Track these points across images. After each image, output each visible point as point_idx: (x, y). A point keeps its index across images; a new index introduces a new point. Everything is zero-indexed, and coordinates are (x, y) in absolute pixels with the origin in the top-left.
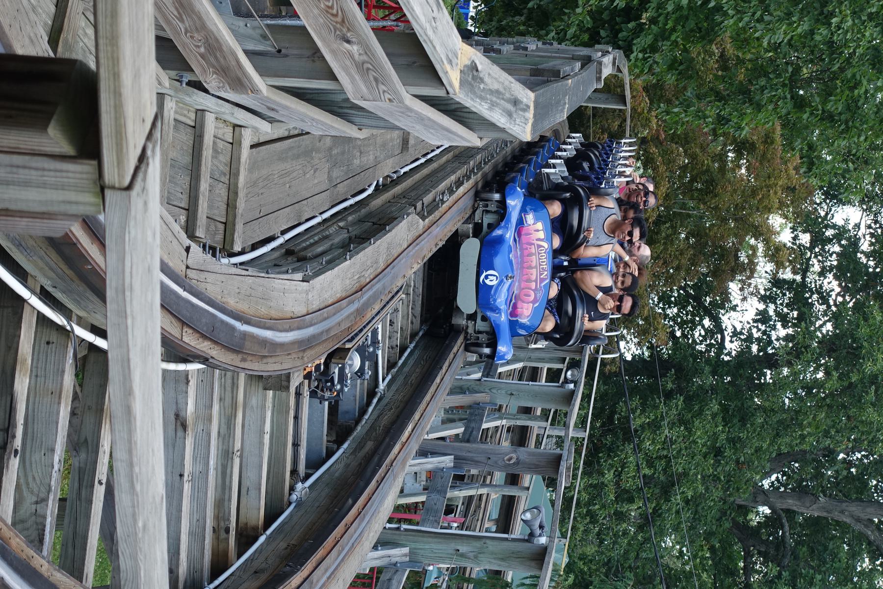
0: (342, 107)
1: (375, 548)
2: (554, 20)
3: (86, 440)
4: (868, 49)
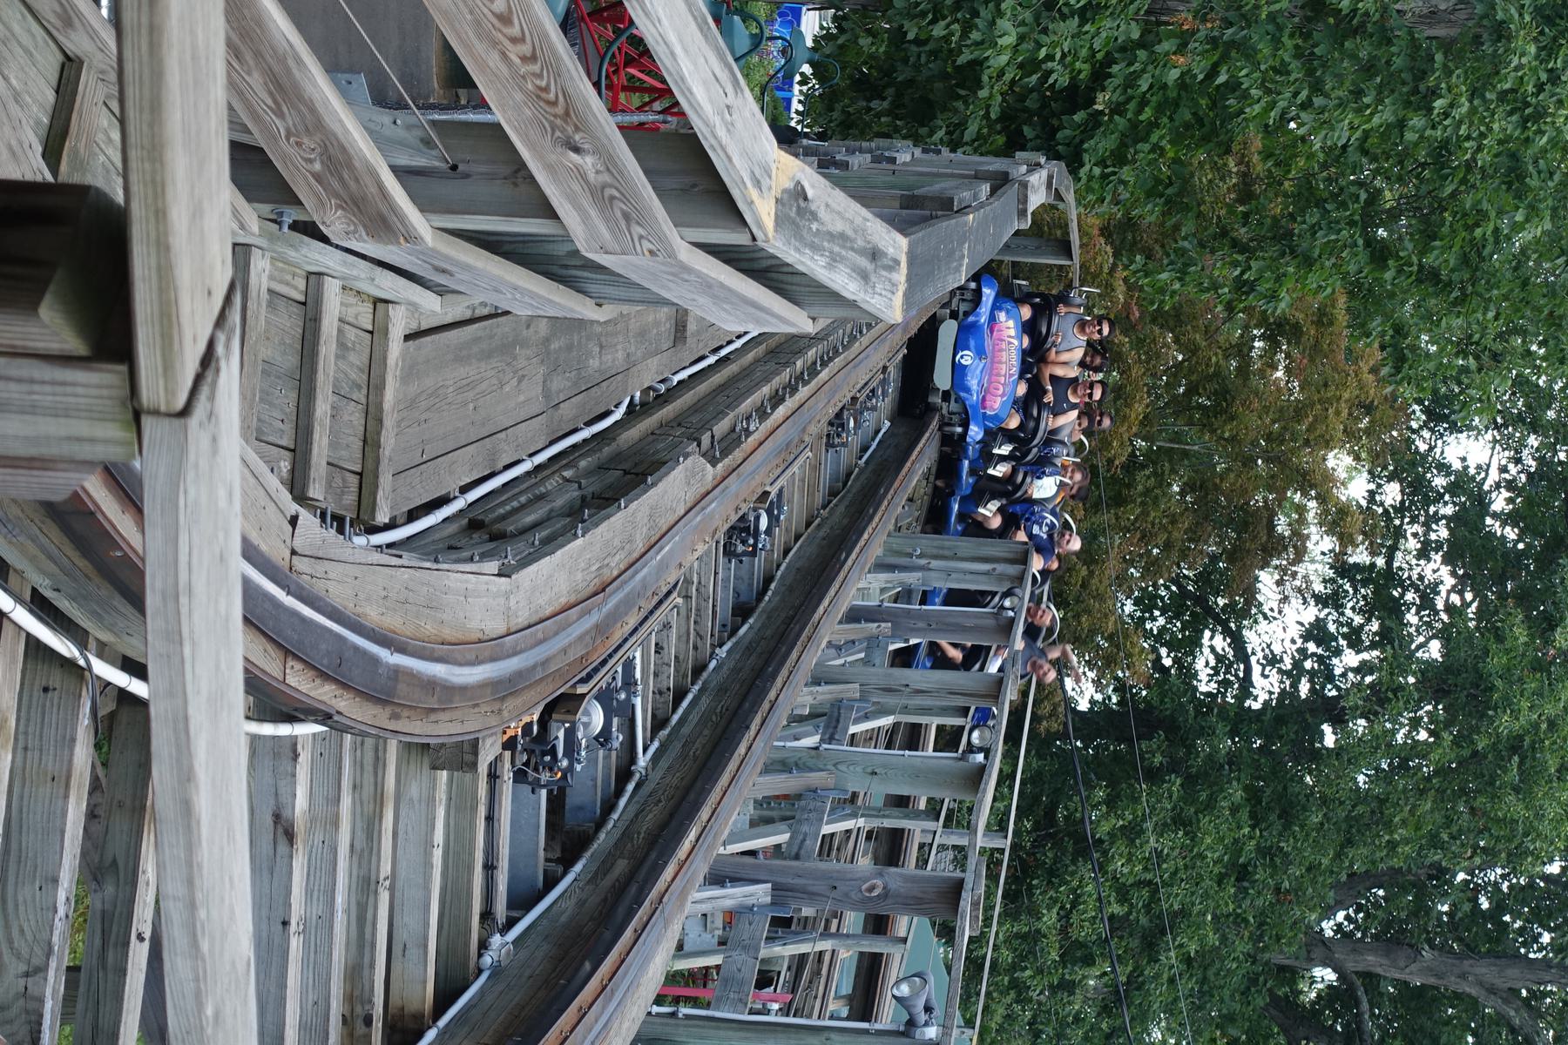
0: (566, 267)
3: (114, 862)
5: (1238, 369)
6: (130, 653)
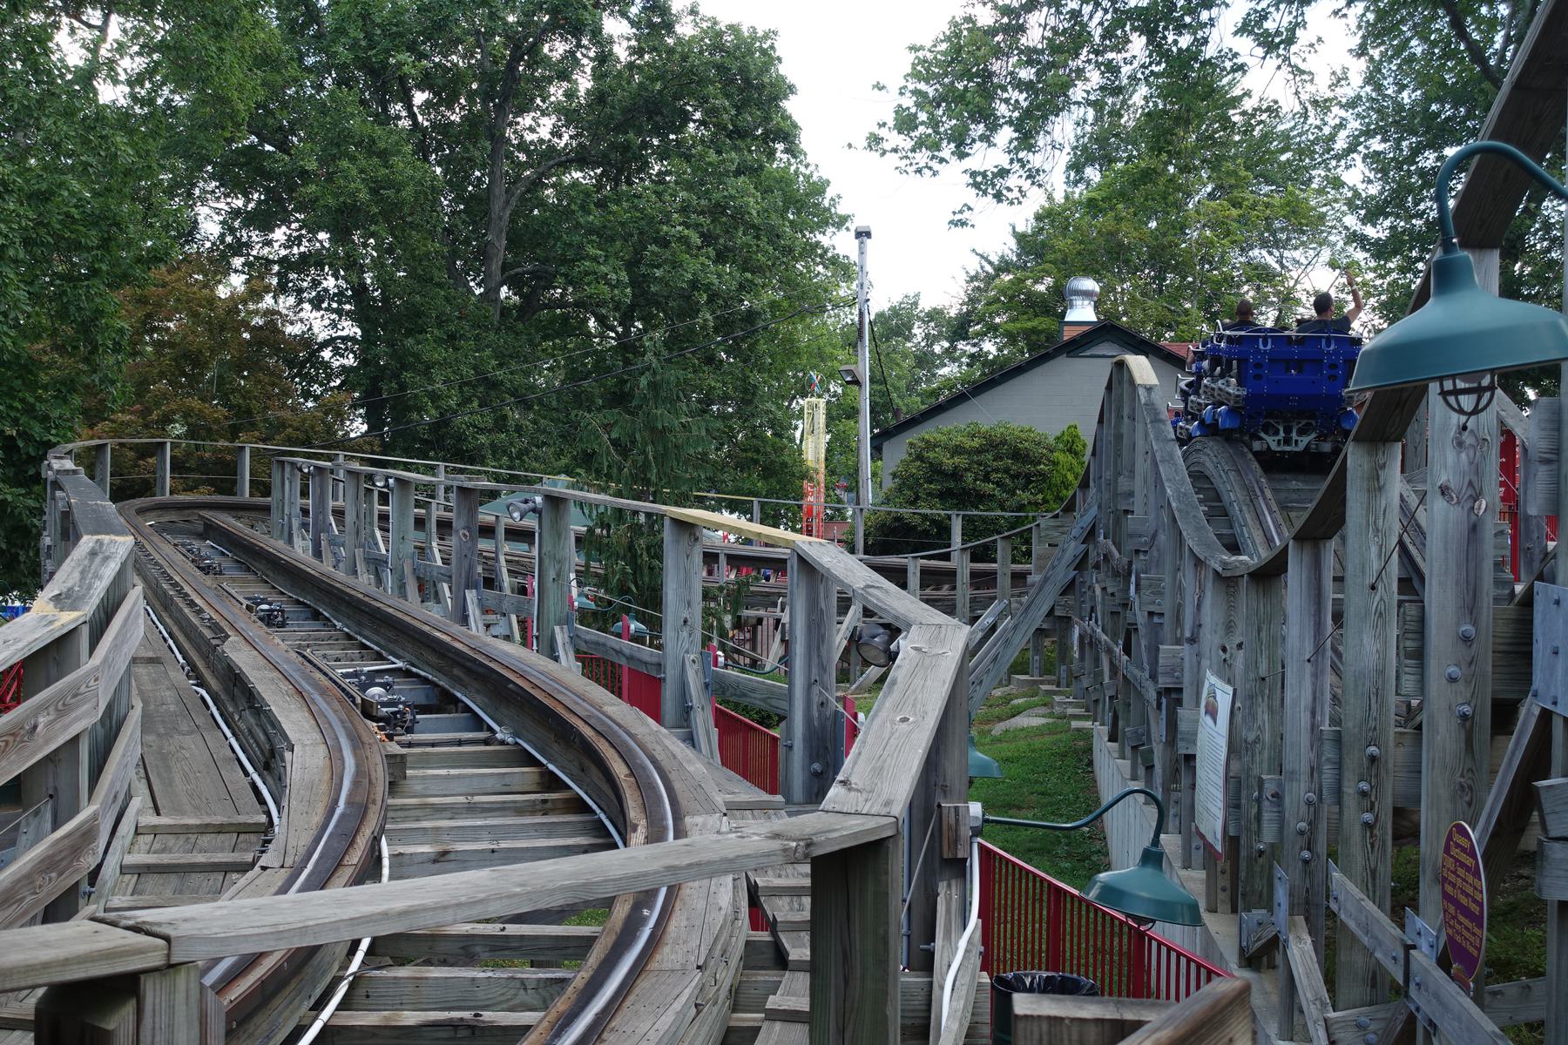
0: (111, 728)
1: (556, 659)
2: (22, 520)
3: (462, 948)
4: (30, 206)
5: (170, 348)
6: (345, 951)
